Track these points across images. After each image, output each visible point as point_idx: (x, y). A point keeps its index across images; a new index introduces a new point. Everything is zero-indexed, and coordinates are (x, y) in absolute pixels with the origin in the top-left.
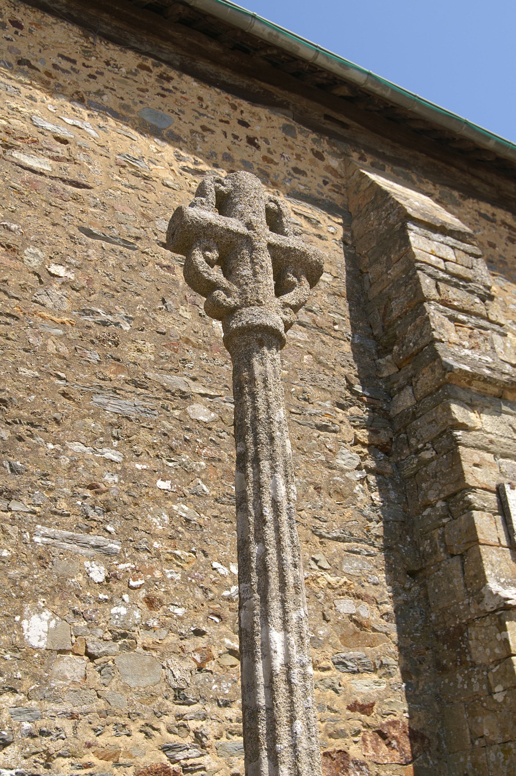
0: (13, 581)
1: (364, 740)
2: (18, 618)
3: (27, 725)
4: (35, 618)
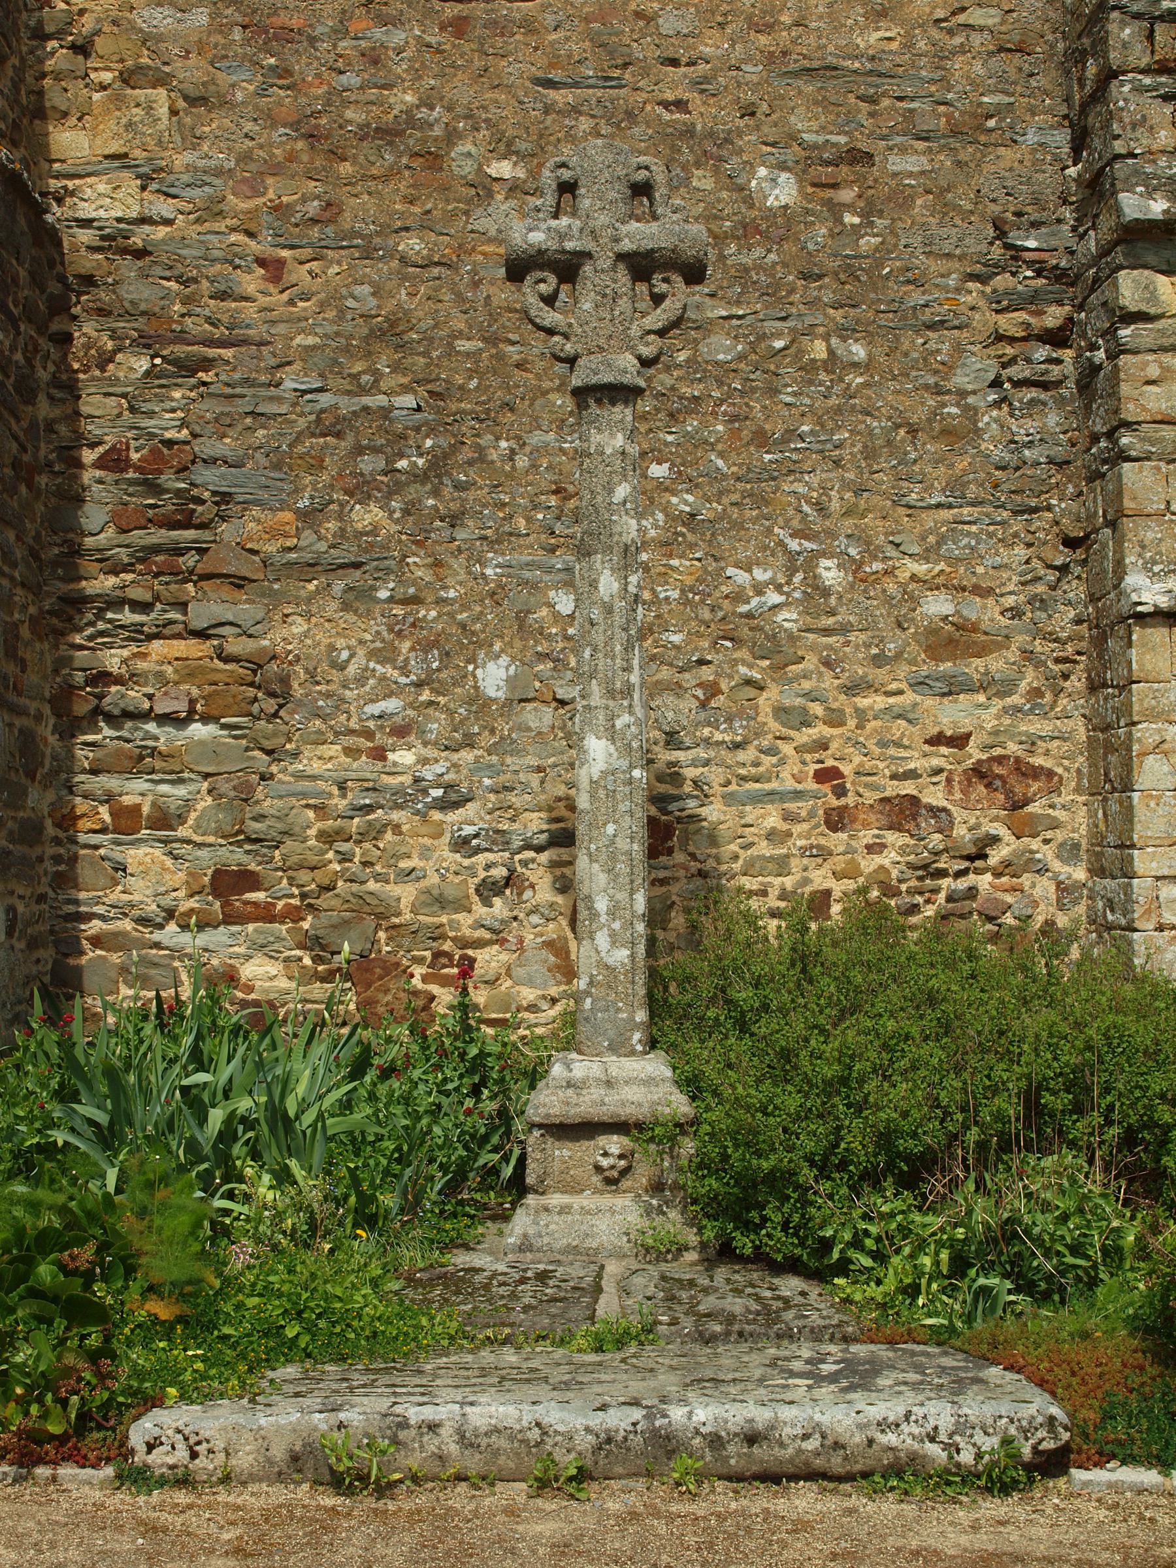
0: (463, 626)
1: (949, 781)
2: (471, 668)
3: (487, 782)
4: (491, 666)
